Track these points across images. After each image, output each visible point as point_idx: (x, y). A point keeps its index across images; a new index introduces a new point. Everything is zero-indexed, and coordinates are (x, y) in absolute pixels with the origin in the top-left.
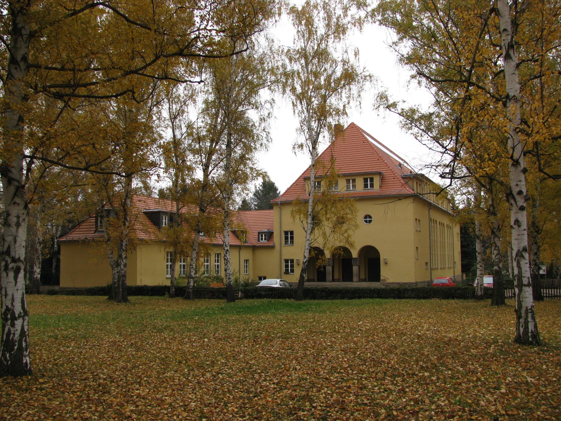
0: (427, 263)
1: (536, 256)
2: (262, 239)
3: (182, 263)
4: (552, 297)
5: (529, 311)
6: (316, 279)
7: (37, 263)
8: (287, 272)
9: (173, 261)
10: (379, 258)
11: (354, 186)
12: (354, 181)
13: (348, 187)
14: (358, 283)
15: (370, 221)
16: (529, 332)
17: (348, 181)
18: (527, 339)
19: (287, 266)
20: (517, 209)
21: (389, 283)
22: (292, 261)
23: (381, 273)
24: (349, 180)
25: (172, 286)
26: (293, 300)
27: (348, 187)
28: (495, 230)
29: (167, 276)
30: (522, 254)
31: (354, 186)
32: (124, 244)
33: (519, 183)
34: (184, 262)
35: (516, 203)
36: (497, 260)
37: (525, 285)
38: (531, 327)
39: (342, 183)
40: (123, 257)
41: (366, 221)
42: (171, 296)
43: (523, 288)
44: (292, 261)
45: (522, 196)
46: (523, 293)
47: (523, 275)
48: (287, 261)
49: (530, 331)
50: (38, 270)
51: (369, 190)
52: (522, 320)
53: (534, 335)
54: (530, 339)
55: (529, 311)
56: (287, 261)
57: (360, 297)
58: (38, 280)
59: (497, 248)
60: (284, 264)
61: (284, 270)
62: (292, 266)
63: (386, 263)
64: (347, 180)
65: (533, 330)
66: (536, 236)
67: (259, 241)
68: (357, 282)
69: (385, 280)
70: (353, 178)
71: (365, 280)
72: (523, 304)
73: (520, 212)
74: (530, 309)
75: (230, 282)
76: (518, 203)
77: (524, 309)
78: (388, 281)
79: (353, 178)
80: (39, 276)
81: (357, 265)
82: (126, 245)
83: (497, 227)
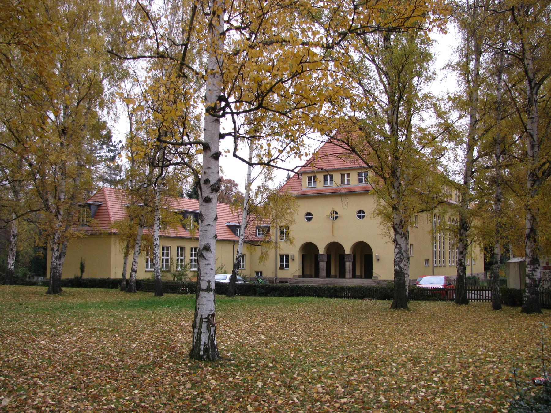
0: (427, 261)
1: (462, 255)
2: (259, 234)
3: (193, 258)
4: (486, 300)
5: (204, 320)
6: (314, 276)
7: (11, 255)
8: (282, 268)
9: (126, 255)
10: (372, 255)
11: (349, 181)
12: (349, 175)
13: (343, 182)
14: (350, 280)
15: (363, 217)
16: (200, 345)
17: (343, 175)
18: (204, 354)
19: (282, 261)
20: (202, 201)
21: (380, 281)
22: (287, 256)
23: (373, 270)
24: (344, 174)
25: (123, 280)
26: (224, 296)
27: (343, 182)
28: (397, 227)
29: (147, 270)
30: (202, 254)
31: (349, 181)
32: (56, 237)
33: (207, 171)
34: (167, 255)
35: (202, 194)
36: (397, 259)
37: (203, 290)
38: (204, 339)
39: (337, 177)
40: (55, 250)
41: (359, 217)
42: (122, 289)
43: (201, 293)
44: (287, 256)
45: (209, 186)
46: (200, 298)
47: (202, 278)
48: (282, 256)
49: (202, 343)
50: (12, 262)
51: (346, 186)
52: (196, 330)
53: (206, 348)
54: (202, 353)
55: (204, 320)
56: (282, 256)
57: (298, 295)
58: (11, 271)
59: (398, 246)
60: (279, 259)
61: (279, 264)
62: (287, 262)
63: (293, 260)
64: (359, 173)
65: (207, 342)
66: (463, 233)
67: (256, 236)
68: (350, 278)
69: (377, 277)
70: (348, 172)
71: (361, 277)
72: (199, 311)
73: (204, 204)
74: (205, 318)
75: (157, 276)
76: (203, 193)
77: (199, 317)
78: (379, 278)
79: (348, 172)
80: (13, 267)
81: (349, 261)
82: (58, 238)
83: (398, 223)
